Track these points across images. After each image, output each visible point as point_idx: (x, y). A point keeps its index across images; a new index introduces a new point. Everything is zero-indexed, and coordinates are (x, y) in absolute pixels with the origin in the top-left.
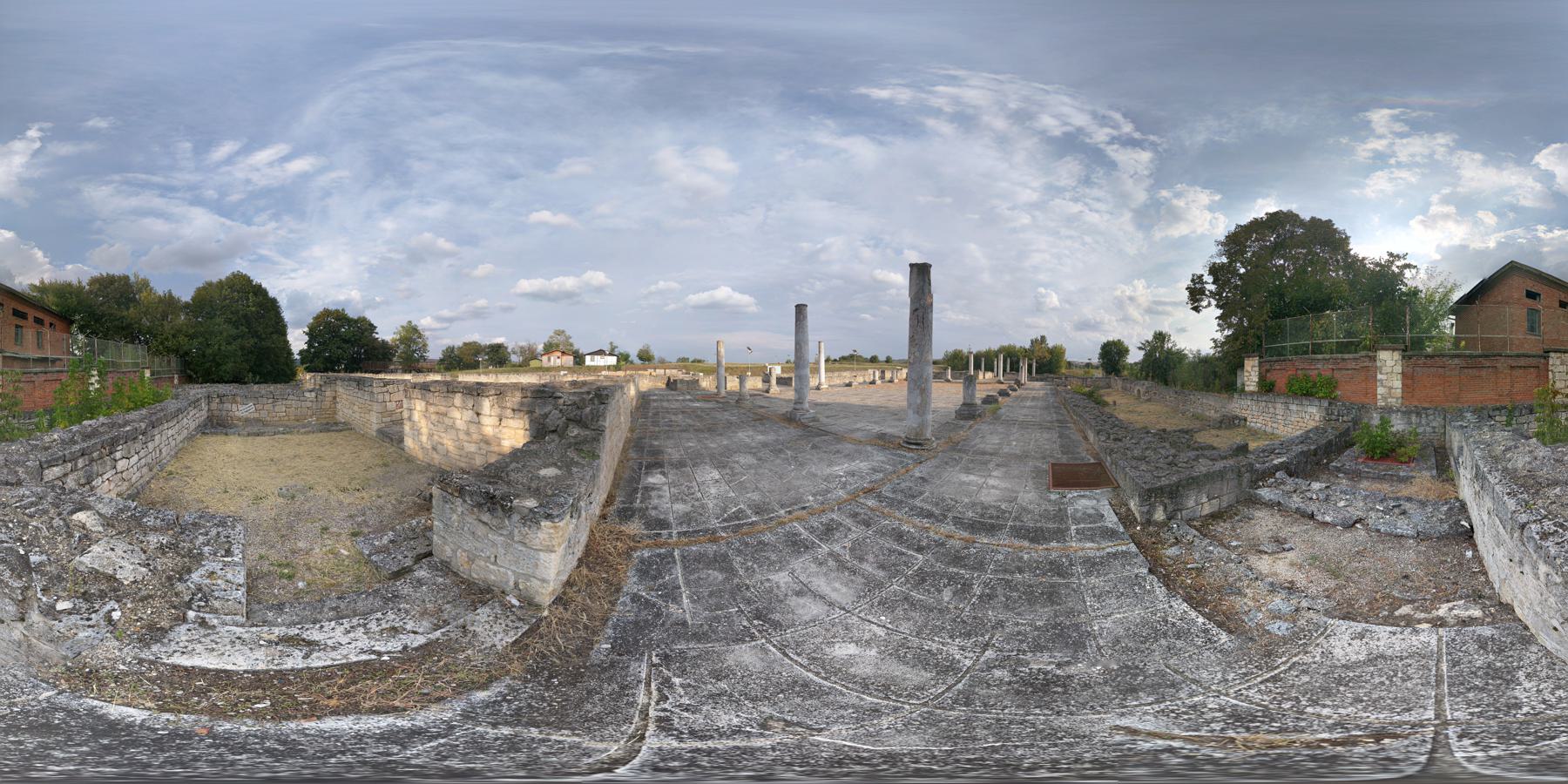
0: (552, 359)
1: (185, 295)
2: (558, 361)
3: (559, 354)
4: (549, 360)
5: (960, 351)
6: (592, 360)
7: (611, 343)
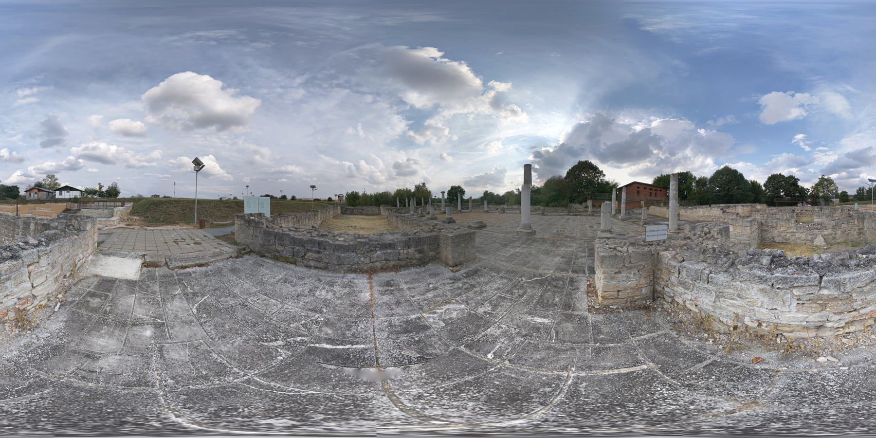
0: (32, 194)
1: (698, 177)
2: (36, 196)
3: (37, 191)
4: (30, 195)
5: (357, 194)
6: (61, 194)
7: (99, 184)
